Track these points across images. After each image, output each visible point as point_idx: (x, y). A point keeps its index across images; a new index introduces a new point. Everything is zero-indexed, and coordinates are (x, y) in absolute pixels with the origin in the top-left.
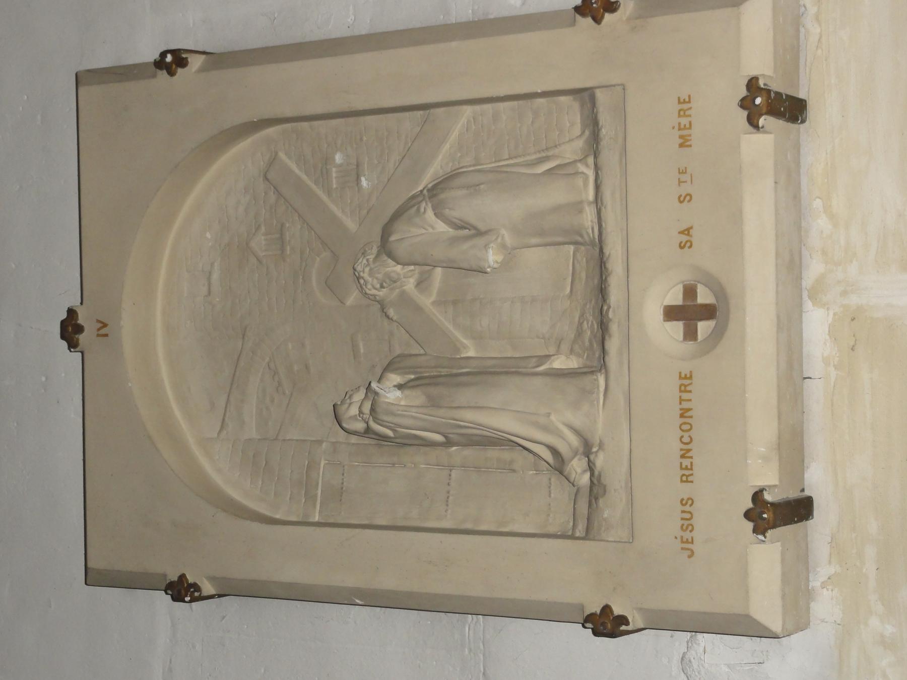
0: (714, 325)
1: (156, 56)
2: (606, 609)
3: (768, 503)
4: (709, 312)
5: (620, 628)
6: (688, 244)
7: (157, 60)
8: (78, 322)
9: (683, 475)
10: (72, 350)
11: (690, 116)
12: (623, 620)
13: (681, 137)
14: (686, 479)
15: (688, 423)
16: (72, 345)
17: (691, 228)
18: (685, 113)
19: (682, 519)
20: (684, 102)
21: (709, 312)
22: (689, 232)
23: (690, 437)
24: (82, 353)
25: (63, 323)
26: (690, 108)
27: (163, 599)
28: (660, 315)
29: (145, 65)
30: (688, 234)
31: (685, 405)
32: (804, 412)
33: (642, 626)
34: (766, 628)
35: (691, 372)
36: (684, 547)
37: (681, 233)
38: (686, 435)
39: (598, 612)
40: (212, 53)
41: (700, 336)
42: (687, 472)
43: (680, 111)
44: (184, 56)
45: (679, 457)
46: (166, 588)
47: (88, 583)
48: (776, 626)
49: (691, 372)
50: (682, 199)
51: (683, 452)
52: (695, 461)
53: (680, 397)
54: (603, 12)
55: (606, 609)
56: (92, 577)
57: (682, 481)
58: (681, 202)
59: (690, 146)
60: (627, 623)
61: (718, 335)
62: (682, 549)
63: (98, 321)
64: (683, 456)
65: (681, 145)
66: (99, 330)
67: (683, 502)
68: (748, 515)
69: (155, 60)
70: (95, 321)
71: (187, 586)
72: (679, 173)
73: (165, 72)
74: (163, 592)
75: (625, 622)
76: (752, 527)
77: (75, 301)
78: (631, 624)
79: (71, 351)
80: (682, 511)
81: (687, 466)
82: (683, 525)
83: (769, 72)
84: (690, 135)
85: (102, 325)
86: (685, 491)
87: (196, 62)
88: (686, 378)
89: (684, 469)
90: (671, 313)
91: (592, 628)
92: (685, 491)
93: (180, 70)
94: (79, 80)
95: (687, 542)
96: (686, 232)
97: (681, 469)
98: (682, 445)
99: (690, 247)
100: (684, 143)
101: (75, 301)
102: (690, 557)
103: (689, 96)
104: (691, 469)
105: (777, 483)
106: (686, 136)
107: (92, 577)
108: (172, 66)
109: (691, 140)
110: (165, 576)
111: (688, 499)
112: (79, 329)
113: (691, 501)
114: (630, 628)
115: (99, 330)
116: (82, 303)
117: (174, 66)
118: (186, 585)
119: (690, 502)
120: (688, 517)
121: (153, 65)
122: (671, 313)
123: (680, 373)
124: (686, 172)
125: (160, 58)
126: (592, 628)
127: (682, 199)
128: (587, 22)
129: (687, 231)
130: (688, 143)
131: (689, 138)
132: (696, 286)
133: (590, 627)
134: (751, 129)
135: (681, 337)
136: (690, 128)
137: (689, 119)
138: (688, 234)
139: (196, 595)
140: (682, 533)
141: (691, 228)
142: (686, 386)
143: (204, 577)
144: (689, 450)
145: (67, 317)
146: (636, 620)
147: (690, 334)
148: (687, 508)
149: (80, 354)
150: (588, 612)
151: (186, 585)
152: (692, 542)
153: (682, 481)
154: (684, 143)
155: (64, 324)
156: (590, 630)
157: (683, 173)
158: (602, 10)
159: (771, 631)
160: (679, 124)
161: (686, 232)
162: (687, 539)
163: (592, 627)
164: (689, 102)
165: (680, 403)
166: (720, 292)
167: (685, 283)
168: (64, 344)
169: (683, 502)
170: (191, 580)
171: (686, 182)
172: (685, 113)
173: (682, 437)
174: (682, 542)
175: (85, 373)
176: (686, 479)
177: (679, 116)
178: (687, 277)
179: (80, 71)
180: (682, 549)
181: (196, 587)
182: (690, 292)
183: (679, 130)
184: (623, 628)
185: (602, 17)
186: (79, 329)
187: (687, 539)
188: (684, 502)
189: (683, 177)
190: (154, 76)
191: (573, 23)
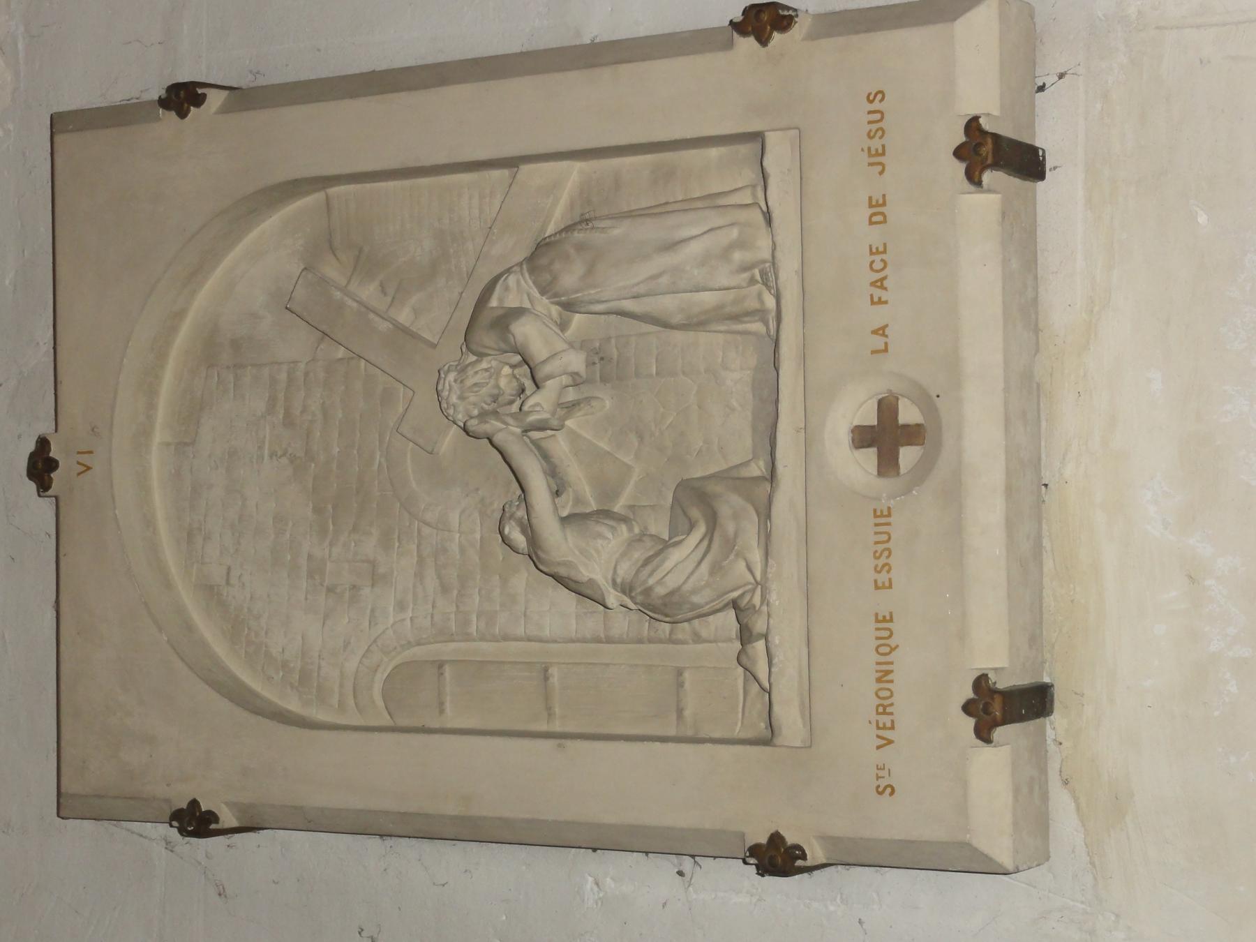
3: (986, 133)
4: (913, 434)
5: (795, 863)
7: (162, 97)
8: (51, 455)
9: (882, 705)
10: (41, 494)
11: (891, 714)
17: (887, 326)
18: (884, 709)
19: (870, 122)
20: (878, 205)
21: (913, 434)
22: (884, 332)
23: (882, 260)
24: (56, 498)
25: (32, 456)
26: (892, 705)
28: (845, 437)
29: (150, 103)
30: (884, 335)
33: (824, 861)
35: (884, 196)
36: (871, 119)
37: (875, 332)
38: (878, 258)
42: (886, 702)
43: (878, 706)
44: (200, 91)
46: (170, 818)
47: (61, 814)
48: (1007, 861)
50: (871, 98)
53: (877, 774)
54: (771, 30)
56: (65, 806)
57: (871, 223)
60: (804, 857)
68: (968, 708)
69: (160, 97)
71: (199, 816)
72: (878, 769)
76: (973, 724)
77: (46, 428)
78: (808, 860)
79: (39, 496)
85: (85, 468)
87: (215, 99)
88: (884, 620)
90: (863, 437)
91: (755, 865)
92: (878, 316)
94: (58, 123)
96: (881, 332)
97: (869, 207)
98: (879, 656)
99: (892, 793)
102: (881, 173)
103: (891, 614)
104: (884, 204)
107: (65, 806)
112: (52, 465)
113: (887, 552)
114: (809, 863)
116: (56, 431)
117: (186, 105)
118: (198, 814)
120: (887, 636)
121: (157, 103)
122: (863, 437)
123: (877, 615)
124: (884, 769)
126: (755, 865)
127: (871, 98)
128: (747, 44)
129: (881, 331)
134: (972, 188)
135: (875, 473)
136: (883, 154)
137: (891, 717)
138: (884, 335)
139: (211, 827)
140: (877, 576)
141: (887, 326)
142: (885, 707)
144: (888, 672)
145: (35, 482)
146: (816, 853)
147: (888, 464)
148: (876, 105)
150: (751, 841)
151: (198, 814)
152: (891, 620)
153: (871, 223)
155: (33, 458)
156: (754, 866)
157: (881, 769)
158: (769, 27)
161: (881, 332)
163: (756, 862)
165: (877, 780)
166: (927, 402)
168: (32, 486)
171: (883, 777)
172: (884, 709)
173: (872, 262)
174: (870, 155)
177: (878, 713)
178: (880, 386)
180: (871, 164)
181: (211, 817)
182: (887, 408)
184: (799, 863)
186: (52, 465)
189: (881, 773)
191: (729, 45)
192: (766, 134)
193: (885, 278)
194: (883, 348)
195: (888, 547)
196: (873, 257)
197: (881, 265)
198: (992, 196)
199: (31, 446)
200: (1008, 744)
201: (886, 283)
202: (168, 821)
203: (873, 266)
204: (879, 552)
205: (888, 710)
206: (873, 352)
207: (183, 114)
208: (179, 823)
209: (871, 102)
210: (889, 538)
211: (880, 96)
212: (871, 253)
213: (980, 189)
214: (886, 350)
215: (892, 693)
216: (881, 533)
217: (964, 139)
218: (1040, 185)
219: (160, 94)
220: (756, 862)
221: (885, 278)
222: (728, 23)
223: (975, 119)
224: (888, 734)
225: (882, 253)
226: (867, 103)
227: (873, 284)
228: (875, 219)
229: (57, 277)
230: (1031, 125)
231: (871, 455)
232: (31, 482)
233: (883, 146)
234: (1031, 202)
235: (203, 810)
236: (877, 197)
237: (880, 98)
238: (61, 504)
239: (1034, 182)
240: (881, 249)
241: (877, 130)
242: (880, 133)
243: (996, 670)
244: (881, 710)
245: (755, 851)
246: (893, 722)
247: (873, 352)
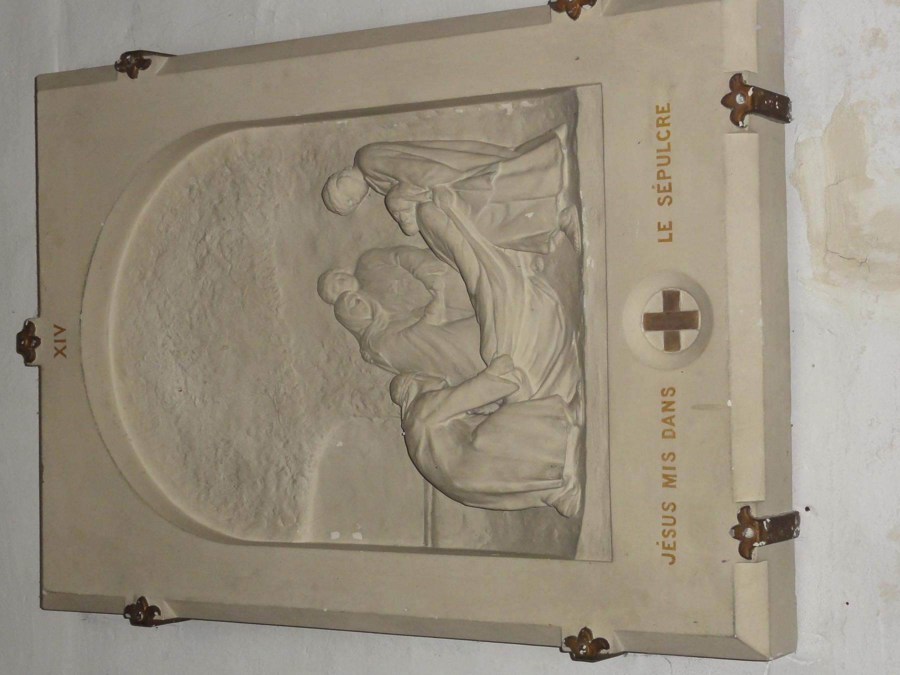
0: (695, 337)
1: (117, 58)
2: (585, 633)
4: (688, 321)
6: (668, 200)
7: (118, 63)
9: (660, 118)
11: (668, 125)
12: (602, 643)
13: (665, 476)
14: (668, 435)
15: (671, 430)
16: (29, 359)
18: (663, 122)
20: (663, 111)
21: (688, 321)
24: (39, 367)
27: (124, 623)
29: (104, 68)
31: (668, 414)
32: (792, 425)
33: (623, 650)
34: (751, 649)
36: (659, 155)
38: (663, 195)
39: (577, 636)
40: (174, 56)
41: (683, 346)
42: (664, 115)
44: (145, 57)
45: (661, 410)
47: (44, 606)
49: (668, 104)
51: (664, 405)
52: (673, 181)
55: (585, 633)
57: (664, 436)
58: (661, 204)
59: (674, 487)
60: (607, 647)
61: (701, 345)
62: (664, 555)
63: (55, 326)
64: (658, 125)
65: (665, 485)
66: (56, 334)
67: (663, 393)
69: (116, 62)
70: (53, 326)
73: (126, 74)
74: (123, 616)
75: (604, 646)
77: (31, 313)
79: (26, 365)
80: (657, 150)
81: (665, 226)
82: (664, 531)
83: (754, 69)
84: (675, 476)
86: (667, 446)
87: (159, 64)
89: (662, 192)
90: (652, 322)
91: (570, 652)
92: (667, 446)
93: (140, 72)
94: (38, 84)
95: (669, 548)
96: (669, 421)
97: (663, 549)
100: (669, 481)
101: (31, 313)
102: (671, 563)
103: (670, 223)
105: (762, 498)
106: (670, 476)
108: (134, 68)
109: (675, 481)
110: (123, 599)
111: (670, 454)
114: (610, 651)
115: (56, 334)
116: (39, 315)
117: (135, 68)
118: (145, 609)
119: (671, 392)
122: (652, 322)
123: (659, 224)
125: (121, 60)
126: (570, 652)
130: (664, 405)
131: (674, 478)
132: (678, 294)
133: (569, 651)
134: (735, 128)
137: (668, 181)
142: (664, 119)
143: (166, 600)
145: (23, 355)
147: (672, 343)
148: (668, 463)
149: (37, 369)
150: (565, 636)
152: (674, 548)
153: (664, 436)
154: (669, 481)
155: (20, 337)
156: (568, 654)
159: (757, 653)
160: (659, 186)
162: (669, 545)
163: (570, 650)
164: (668, 111)
167: (665, 289)
168: (20, 358)
169: (663, 393)
170: (150, 603)
172: (663, 122)
174: (664, 548)
175: (43, 423)
176: (668, 435)
177: (659, 178)
179: (40, 75)
180: (664, 555)
182: (671, 298)
183: (657, 126)
184: (603, 652)
185: (578, 13)
187: (669, 545)
188: (665, 457)
190: (116, 78)
191: (549, 20)
192: (578, 89)
193: (674, 417)
194: (667, 148)
195: (668, 155)
196: (660, 129)
197: (666, 135)
198: (754, 136)
199: (20, 328)
200: (755, 132)
201: (674, 420)
202: (123, 613)
203: (660, 136)
204: (666, 391)
205: (666, 122)
206: (660, 241)
207: (132, 75)
208: (131, 615)
209: (666, 510)
210: (669, 162)
211: (671, 457)
212: (659, 191)
213: (747, 560)
214: (670, 239)
215: (674, 433)
216: (667, 517)
217: (730, 91)
218: (787, 125)
219: (117, 60)
220: (570, 650)
221: (674, 417)
222: (547, 3)
223: (739, 76)
224: (668, 427)
225: (666, 112)
226: (658, 205)
227: (664, 421)
228: (667, 434)
229: (41, 280)
230: (782, 82)
231: (660, 335)
232: (19, 355)
233: (675, 543)
234: (780, 140)
235: (149, 606)
236: (664, 223)
237: (672, 458)
238: (43, 373)
239: (783, 124)
240: (667, 227)
241: (666, 395)
242: (672, 534)
243: (757, 503)
244: (660, 122)
245: (569, 641)
246: (670, 184)
247: (660, 241)
